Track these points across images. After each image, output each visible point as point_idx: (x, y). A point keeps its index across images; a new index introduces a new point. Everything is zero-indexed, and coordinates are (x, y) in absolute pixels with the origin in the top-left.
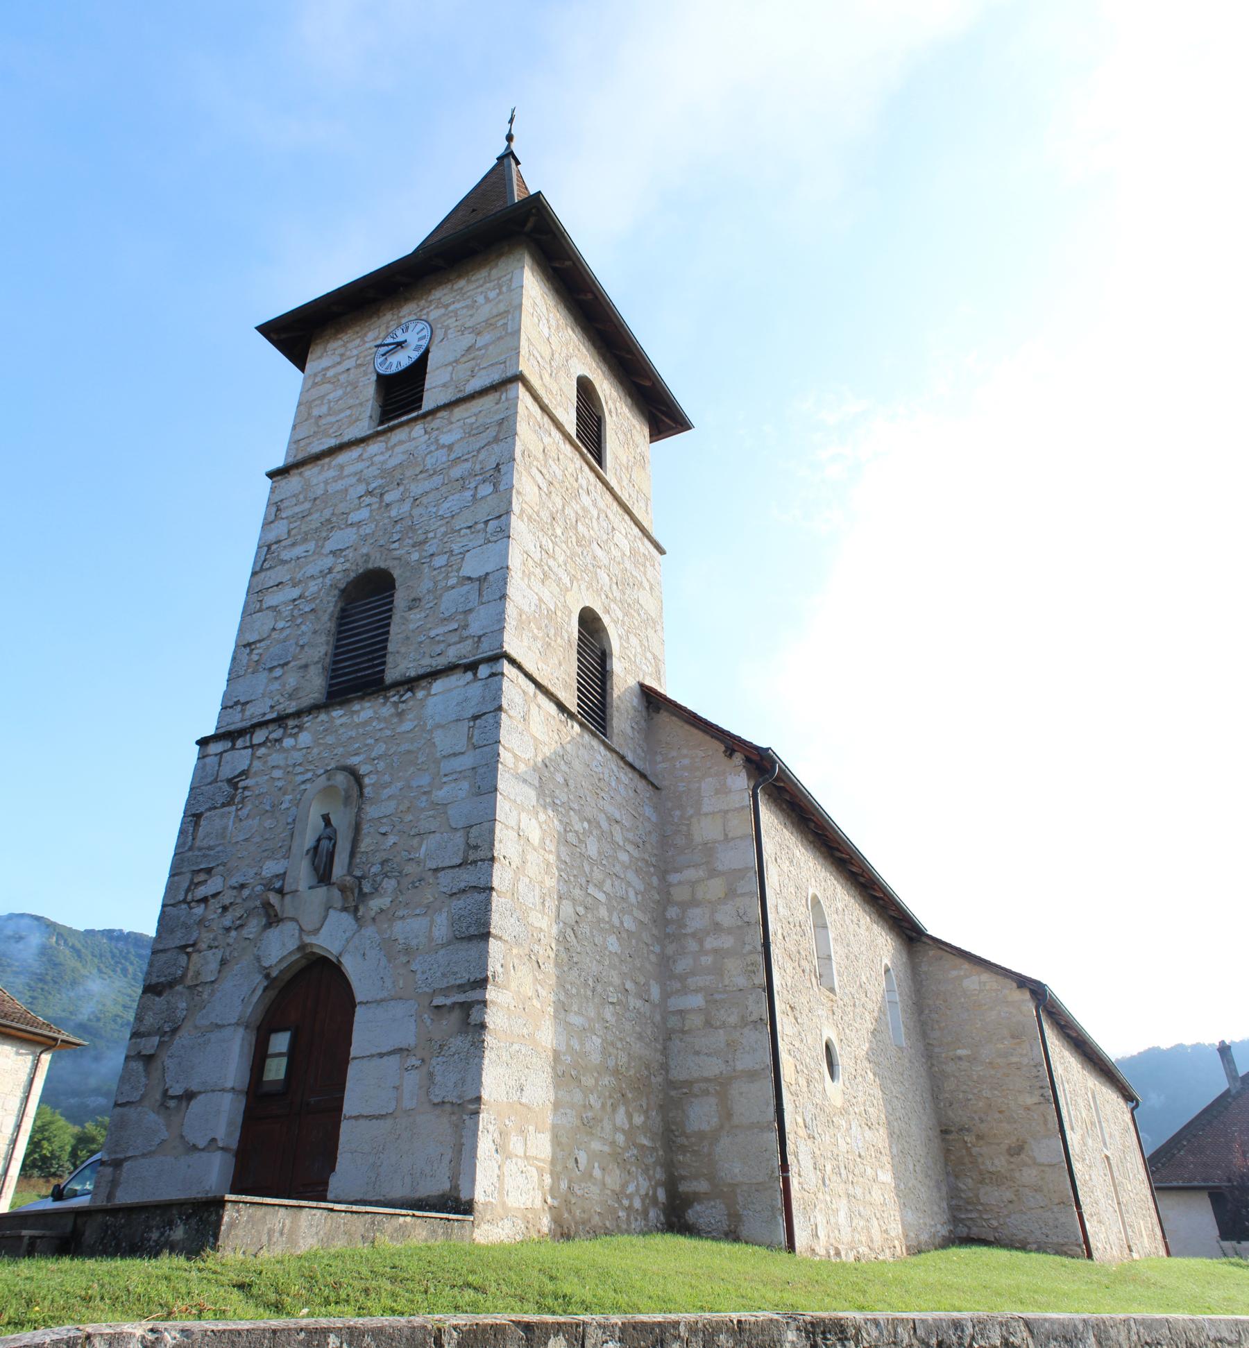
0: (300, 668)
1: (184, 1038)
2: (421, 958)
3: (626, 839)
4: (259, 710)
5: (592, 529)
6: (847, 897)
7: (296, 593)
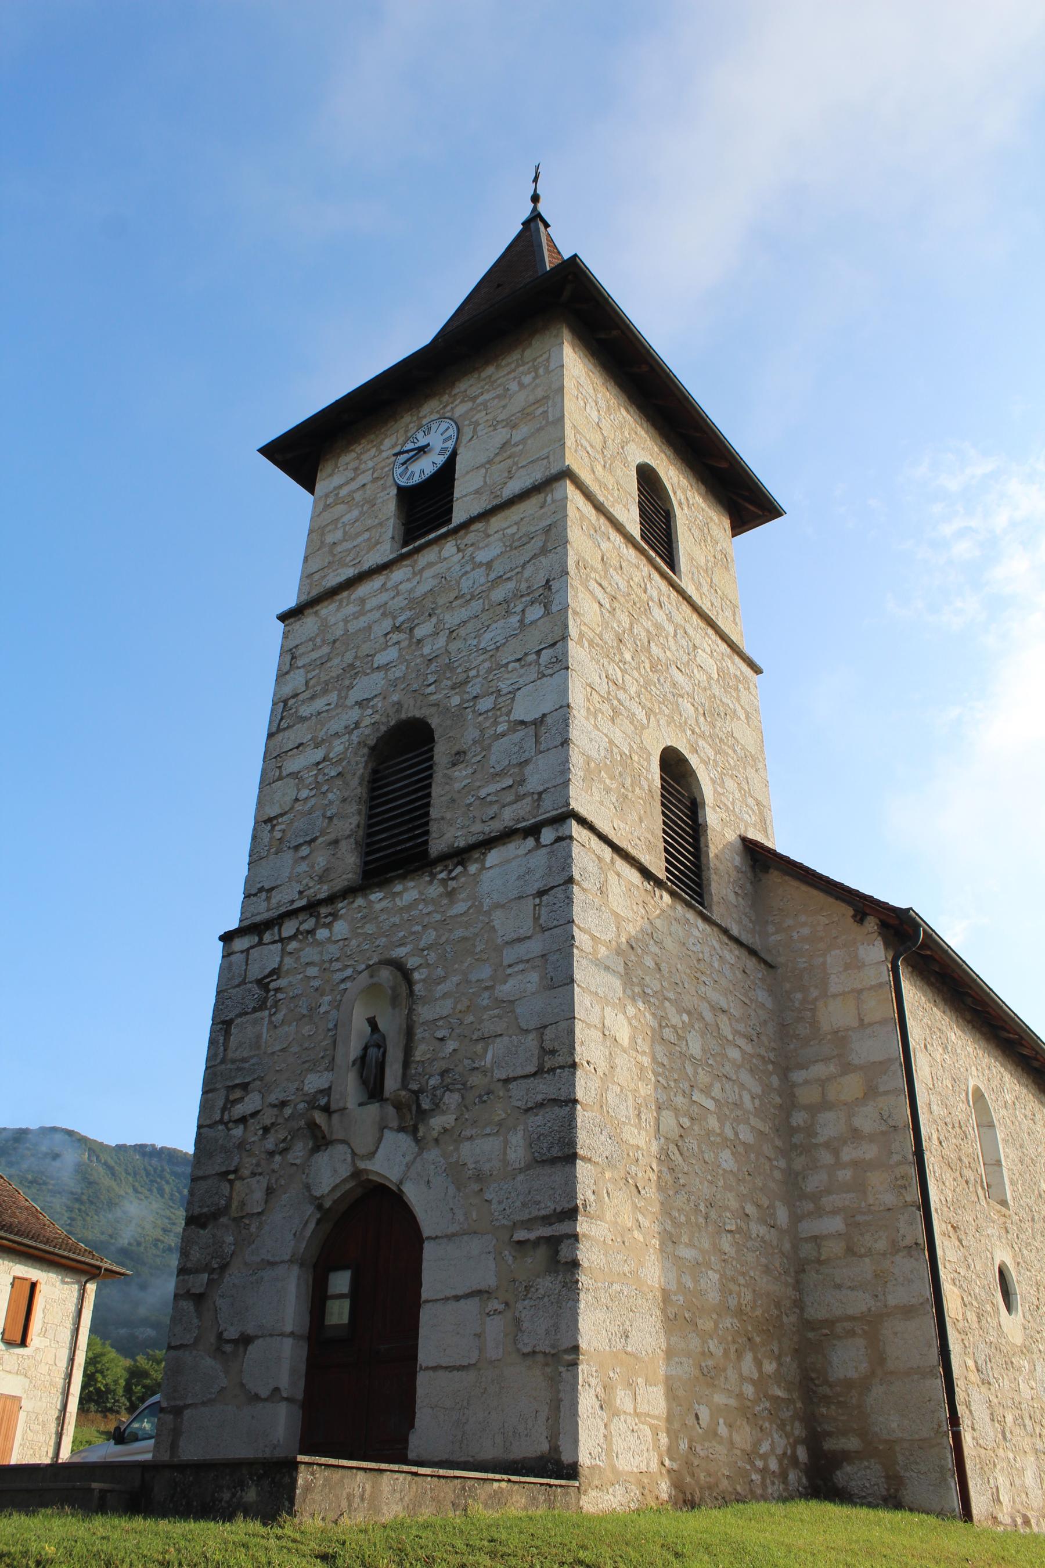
0: (330, 844)
1: (235, 1276)
2: (496, 1185)
3: (736, 1032)
4: (287, 896)
5: (669, 649)
6: (1017, 1088)
7: (319, 754)
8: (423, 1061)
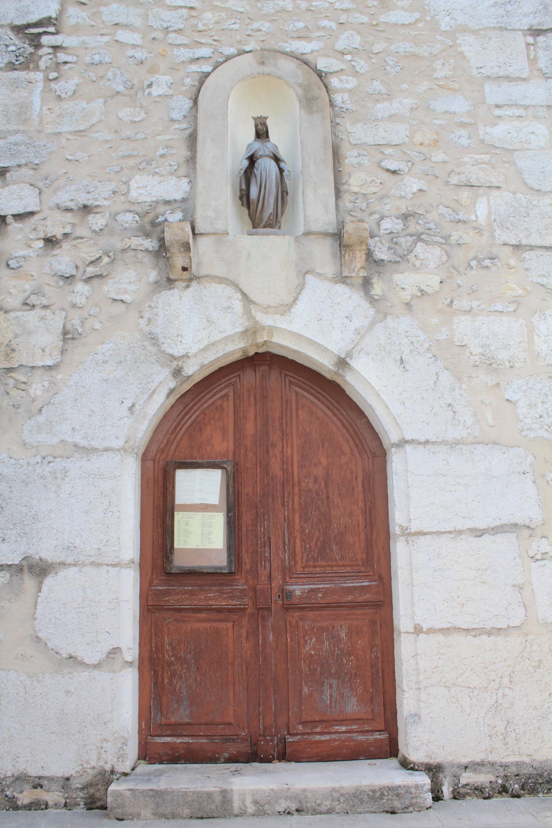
8: (364, 195)
